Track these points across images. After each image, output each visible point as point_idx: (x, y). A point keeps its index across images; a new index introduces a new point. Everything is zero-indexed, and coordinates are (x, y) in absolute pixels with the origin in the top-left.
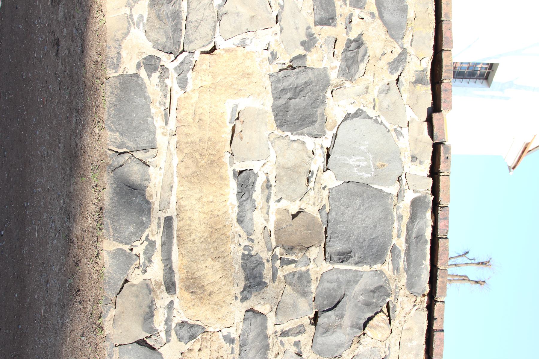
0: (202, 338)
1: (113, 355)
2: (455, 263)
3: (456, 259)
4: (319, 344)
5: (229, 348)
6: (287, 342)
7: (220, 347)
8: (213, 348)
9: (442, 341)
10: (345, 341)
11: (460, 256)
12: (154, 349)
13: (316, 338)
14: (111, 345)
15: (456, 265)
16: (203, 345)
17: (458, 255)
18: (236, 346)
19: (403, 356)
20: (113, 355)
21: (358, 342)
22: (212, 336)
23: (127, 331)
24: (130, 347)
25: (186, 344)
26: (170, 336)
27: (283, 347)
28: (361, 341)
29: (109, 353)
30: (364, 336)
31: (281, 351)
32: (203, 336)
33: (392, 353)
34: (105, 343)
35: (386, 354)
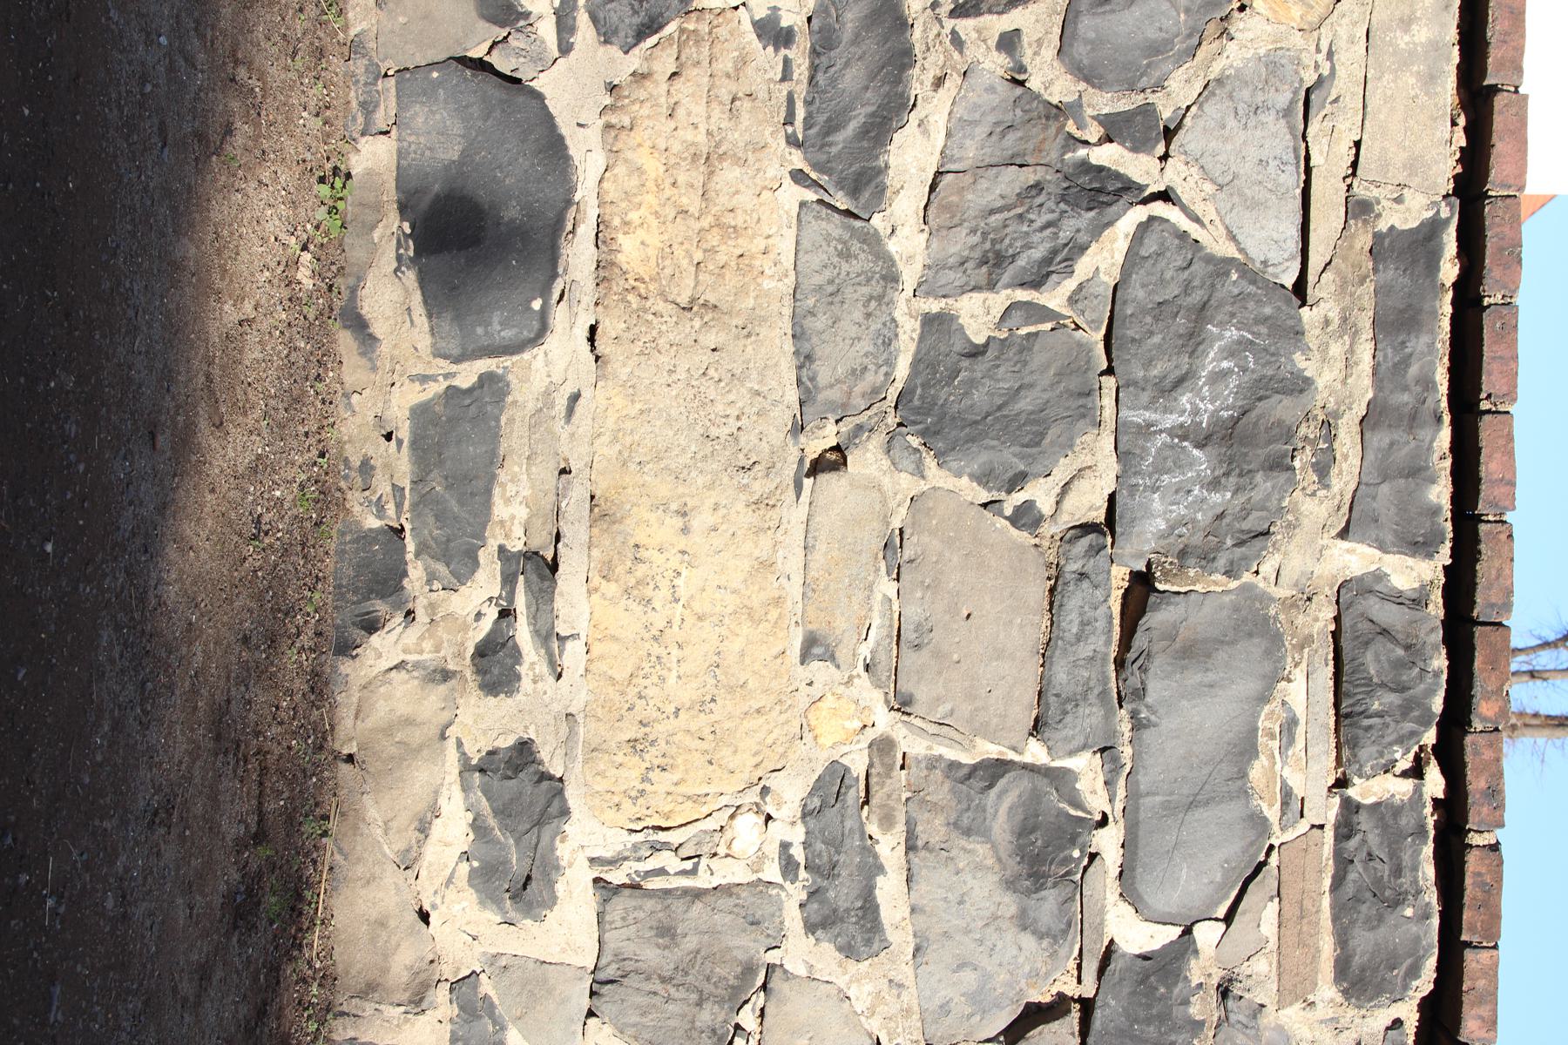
0: (682, 31)
1: (377, 106)
2: (1531, 668)
3: (1532, 656)
4: (1087, 42)
5: (773, 63)
6: (974, 35)
7: (743, 61)
8: (721, 66)
9: (1492, 972)
10: (1175, 29)
11: (1546, 645)
12: (518, 81)
13: (1076, 17)
14: (371, 69)
15: (1532, 674)
16: (683, 57)
17: (1539, 642)
18: (799, 54)
19: (1379, 79)
20: (376, 107)
21: (1222, 33)
22: (715, 23)
23: (426, 17)
24: (435, 75)
25: (626, 53)
26: (572, 30)
27: (961, 52)
28: (1232, 30)
29: (361, 99)
30: (1243, 14)
31: (954, 68)
32: (685, 25)
33: (1341, 72)
34: (351, 62)
35: (1321, 71)
